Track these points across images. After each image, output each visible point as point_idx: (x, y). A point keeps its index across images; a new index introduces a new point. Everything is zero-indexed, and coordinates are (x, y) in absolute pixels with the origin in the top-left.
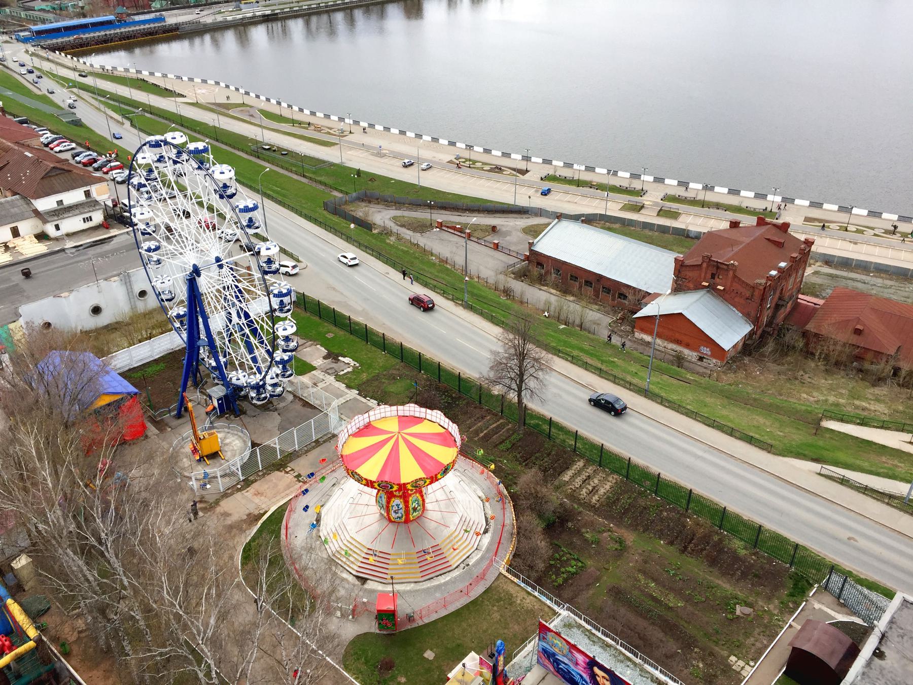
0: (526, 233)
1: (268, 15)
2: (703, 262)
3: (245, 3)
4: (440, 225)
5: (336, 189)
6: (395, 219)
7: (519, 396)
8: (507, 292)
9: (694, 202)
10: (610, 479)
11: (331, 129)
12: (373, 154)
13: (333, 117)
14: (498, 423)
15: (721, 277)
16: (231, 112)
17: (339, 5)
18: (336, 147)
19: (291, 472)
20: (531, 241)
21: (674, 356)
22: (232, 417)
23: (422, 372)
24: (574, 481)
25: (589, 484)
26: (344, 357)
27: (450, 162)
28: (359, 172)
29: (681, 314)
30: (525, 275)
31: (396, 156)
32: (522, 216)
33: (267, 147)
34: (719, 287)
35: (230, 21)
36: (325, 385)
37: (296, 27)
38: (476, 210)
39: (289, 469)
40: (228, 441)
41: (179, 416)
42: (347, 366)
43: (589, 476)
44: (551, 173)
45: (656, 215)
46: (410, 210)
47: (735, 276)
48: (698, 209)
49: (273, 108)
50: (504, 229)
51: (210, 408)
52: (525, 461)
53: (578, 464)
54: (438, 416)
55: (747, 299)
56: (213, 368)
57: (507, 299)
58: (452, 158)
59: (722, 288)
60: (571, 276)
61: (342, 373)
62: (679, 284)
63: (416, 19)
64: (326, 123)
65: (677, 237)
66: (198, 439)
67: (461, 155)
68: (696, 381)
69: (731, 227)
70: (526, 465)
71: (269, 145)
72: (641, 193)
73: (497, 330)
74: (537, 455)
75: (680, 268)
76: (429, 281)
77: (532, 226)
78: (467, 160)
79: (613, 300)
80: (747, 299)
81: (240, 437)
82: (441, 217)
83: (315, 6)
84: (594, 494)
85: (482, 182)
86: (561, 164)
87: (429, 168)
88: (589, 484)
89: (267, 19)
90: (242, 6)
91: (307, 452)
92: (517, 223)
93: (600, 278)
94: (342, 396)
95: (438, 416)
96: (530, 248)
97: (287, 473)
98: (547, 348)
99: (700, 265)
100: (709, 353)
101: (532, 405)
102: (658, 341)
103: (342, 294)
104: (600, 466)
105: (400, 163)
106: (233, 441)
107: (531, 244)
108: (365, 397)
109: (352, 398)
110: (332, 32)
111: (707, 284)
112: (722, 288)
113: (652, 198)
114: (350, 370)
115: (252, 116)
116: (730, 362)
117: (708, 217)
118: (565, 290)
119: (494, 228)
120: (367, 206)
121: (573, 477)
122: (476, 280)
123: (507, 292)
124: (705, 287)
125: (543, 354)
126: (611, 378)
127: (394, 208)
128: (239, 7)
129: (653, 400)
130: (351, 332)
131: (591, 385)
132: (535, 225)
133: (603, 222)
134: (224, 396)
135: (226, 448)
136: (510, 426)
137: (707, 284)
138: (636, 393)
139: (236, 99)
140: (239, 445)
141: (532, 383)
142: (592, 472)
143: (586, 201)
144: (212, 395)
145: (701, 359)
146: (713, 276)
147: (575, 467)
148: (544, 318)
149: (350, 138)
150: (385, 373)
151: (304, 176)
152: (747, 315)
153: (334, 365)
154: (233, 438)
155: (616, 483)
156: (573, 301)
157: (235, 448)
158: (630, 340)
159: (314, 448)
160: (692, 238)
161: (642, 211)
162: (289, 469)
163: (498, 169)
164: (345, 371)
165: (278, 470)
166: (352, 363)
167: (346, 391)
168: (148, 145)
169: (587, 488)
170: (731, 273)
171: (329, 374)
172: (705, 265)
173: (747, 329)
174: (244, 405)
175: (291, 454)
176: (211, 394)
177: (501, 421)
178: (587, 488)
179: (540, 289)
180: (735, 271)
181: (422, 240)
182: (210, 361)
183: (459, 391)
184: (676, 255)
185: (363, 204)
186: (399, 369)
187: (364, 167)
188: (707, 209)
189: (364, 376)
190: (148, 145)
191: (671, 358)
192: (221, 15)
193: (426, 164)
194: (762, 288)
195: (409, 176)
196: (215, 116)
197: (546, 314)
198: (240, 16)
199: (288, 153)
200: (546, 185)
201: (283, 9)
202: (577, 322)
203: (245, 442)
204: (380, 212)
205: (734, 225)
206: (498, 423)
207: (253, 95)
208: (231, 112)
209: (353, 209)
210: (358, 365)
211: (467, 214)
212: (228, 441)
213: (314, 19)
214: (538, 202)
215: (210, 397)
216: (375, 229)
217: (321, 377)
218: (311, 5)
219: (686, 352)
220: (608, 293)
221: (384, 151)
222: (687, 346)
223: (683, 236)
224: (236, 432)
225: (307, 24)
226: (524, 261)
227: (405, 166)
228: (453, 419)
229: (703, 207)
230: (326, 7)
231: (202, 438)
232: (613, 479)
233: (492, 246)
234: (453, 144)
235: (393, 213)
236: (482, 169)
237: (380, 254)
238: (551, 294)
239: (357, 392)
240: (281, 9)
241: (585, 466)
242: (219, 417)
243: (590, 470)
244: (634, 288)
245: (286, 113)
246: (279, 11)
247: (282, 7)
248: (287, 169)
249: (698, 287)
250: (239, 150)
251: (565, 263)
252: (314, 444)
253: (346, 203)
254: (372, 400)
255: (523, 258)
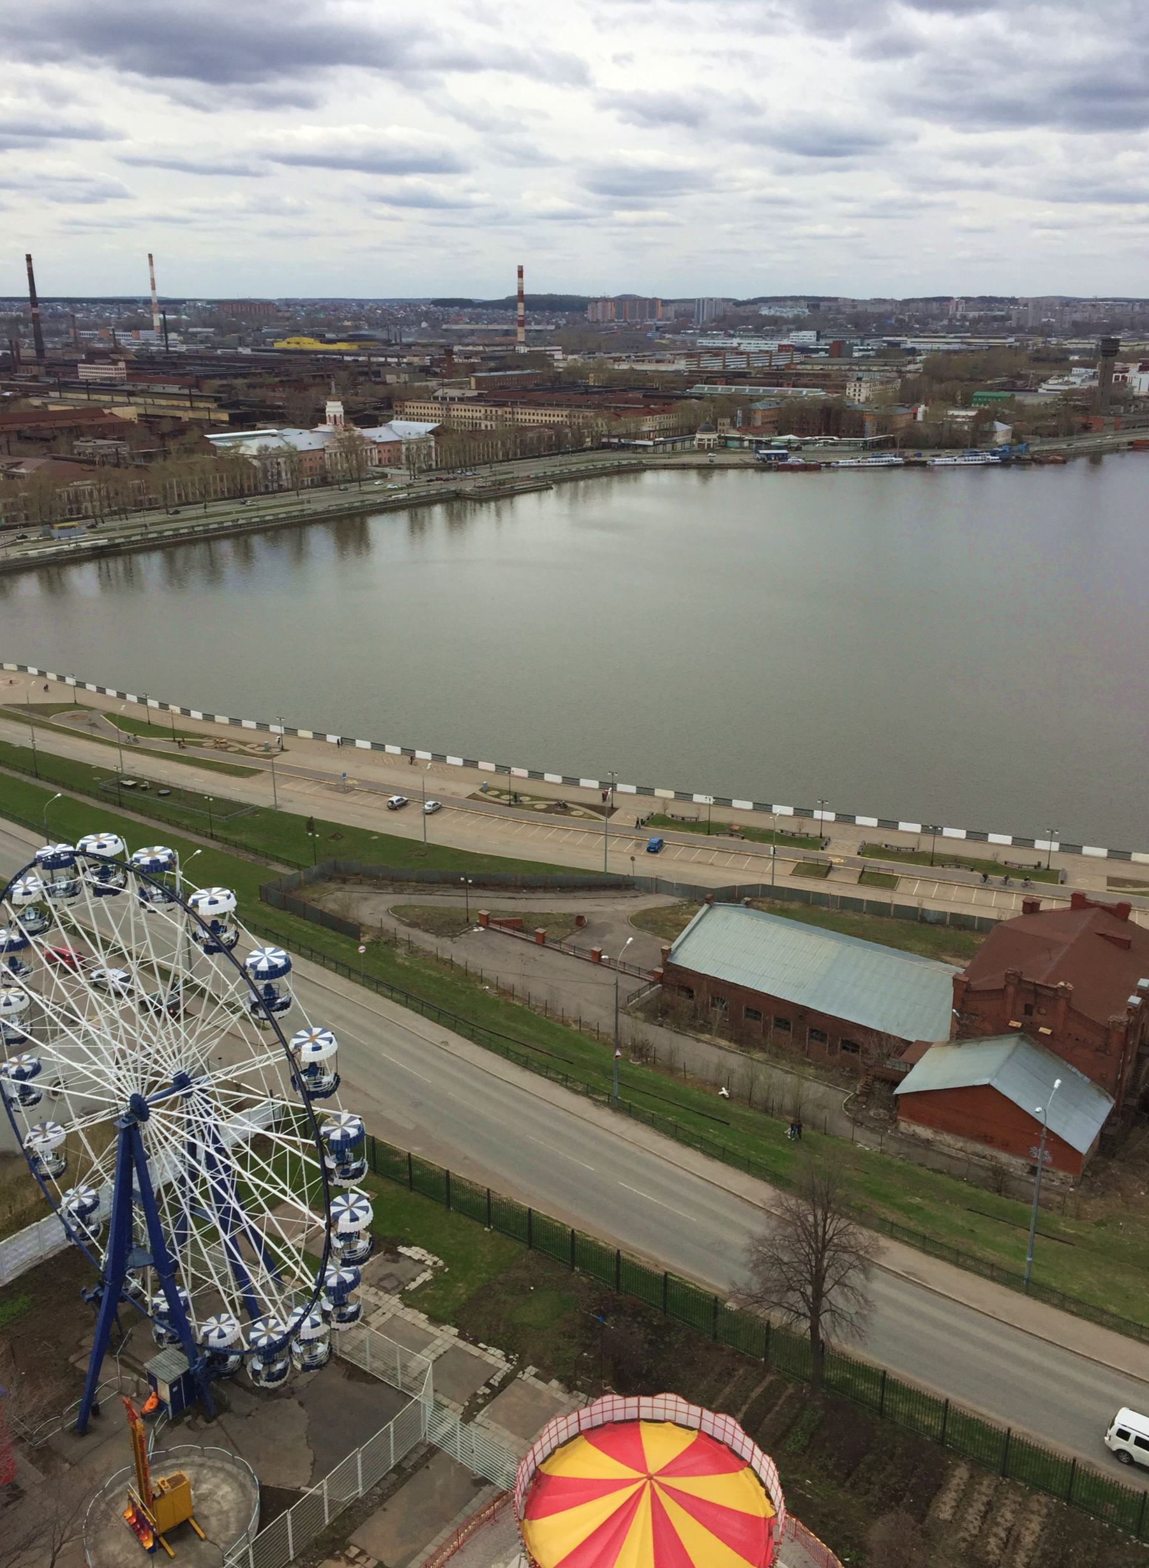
0: (639, 926)
1: (103, 547)
2: (1008, 984)
3: (60, 528)
4: (486, 921)
5: (278, 860)
6: (396, 910)
7: (814, 1329)
8: (641, 1050)
9: (914, 856)
10: (1035, 1506)
11: (245, 744)
12: (330, 788)
13: (246, 723)
14: (765, 1383)
15: (1043, 1011)
16: (53, 720)
17: (227, 528)
18: (258, 777)
19: (362, 1559)
20: (666, 947)
21: (988, 1169)
22: (201, 1422)
23: (577, 1269)
24: (963, 1519)
25: (998, 1524)
26: (409, 1245)
27: (474, 797)
28: (311, 823)
29: (988, 1087)
30: (665, 1014)
31: (375, 789)
32: (624, 893)
33: (130, 783)
34: (1042, 1030)
35: (33, 558)
36: (383, 1320)
37: (151, 565)
38: (540, 887)
39: (354, 1551)
40: (205, 1488)
41: (82, 1430)
42: (420, 1267)
43: (989, 1503)
44: (657, 810)
45: (856, 882)
46: (420, 891)
47: (1070, 1009)
48: (923, 869)
49: (129, 706)
50: (597, 921)
51: (150, 1405)
52: (848, 1475)
53: (957, 1473)
54: (729, 1429)
55: (1097, 1050)
56: (162, 1315)
57: (643, 1065)
58: (475, 789)
59: (1048, 1032)
60: (748, 1010)
61: (413, 1286)
62: (966, 1026)
63: (359, 553)
64: (233, 733)
65: (905, 921)
66: (150, 1499)
67: (492, 784)
68: (1081, 1237)
69: (1024, 911)
70: (853, 1486)
71: (133, 778)
72: (820, 842)
73: (761, 1191)
74: (869, 1458)
75: (964, 994)
76: (513, 1047)
77: (646, 912)
78: (502, 792)
79: (832, 1053)
80: (1097, 1050)
81: (230, 1474)
82: (486, 903)
83: (186, 531)
84: (1015, 1550)
85: (536, 832)
86: (671, 794)
87: (437, 809)
88: (998, 1524)
89: (98, 554)
90: (55, 532)
91: (384, 1498)
92: (620, 908)
93: (804, 1012)
94: (425, 1345)
95: (729, 1429)
96: (665, 960)
97: (352, 1561)
98: (864, 1218)
99: (1002, 991)
100: (1049, 1159)
101: (839, 1341)
102: (948, 1138)
103: (367, 1094)
104: (1004, 1476)
105: (382, 803)
106: (217, 1486)
107: (667, 953)
108: (475, 1343)
109: (447, 1347)
110: (213, 571)
111: (1019, 1024)
112: (1048, 1032)
113: (841, 850)
114: (427, 1276)
115: (93, 725)
116: (1089, 1174)
117: (945, 882)
118: (743, 1040)
119: (580, 920)
120: (340, 890)
121: (961, 1506)
122: (575, 1027)
123: (641, 1050)
124: (1016, 1029)
125: (864, 1236)
126: (946, 1253)
127: (390, 890)
128: (49, 534)
129: (1044, 1301)
130: (412, 1184)
131: (914, 1274)
132: (650, 910)
133: (768, 900)
134: (183, 1375)
135: (204, 1509)
136: (791, 1390)
137: (1019, 1024)
138: (1004, 1284)
139: (61, 696)
140: (231, 1497)
141: (835, 1297)
142: (990, 1491)
143: (730, 861)
144: (159, 1374)
145: (1033, 1171)
146: (1028, 1010)
147: (955, 1481)
148: (724, 1102)
149: (282, 759)
150: (501, 1277)
151: (212, 837)
152: (1103, 1083)
153: (391, 1268)
154: (214, 1480)
155: (1049, 1515)
156: (766, 1062)
157: (226, 1507)
158: (891, 1138)
159: (395, 1487)
160: (931, 923)
161: (831, 876)
162: (354, 1551)
163: (562, 807)
164: (419, 1280)
165: (330, 1555)
166: (430, 1260)
167: (432, 1329)
168: (40, 866)
169: (996, 1535)
170: (1062, 1005)
171: (387, 1291)
172: (1011, 989)
173: (1105, 1107)
174: (233, 1396)
175: (350, 1509)
176: (154, 1371)
177: (770, 1378)
178: (996, 1535)
179: (698, 1040)
180: (1068, 1000)
181: (459, 951)
182: (156, 1300)
183: (665, 1311)
184: (953, 969)
185: (332, 886)
186: (527, 1267)
187: (319, 814)
188: (940, 868)
189: (462, 1290)
190: (40, 866)
191: (983, 1174)
192: (18, 548)
193: (431, 803)
194: (1122, 1030)
195: (405, 826)
196: (25, 729)
197: (724, 1092)
198: (53, 549)
199: (174, 793)
200: (654, 834)
201: (130, 536)
202: (788, 1102)
203: (242, 1487)
204: (366, 899)
205: (1031, 908)
206: (765, 1383)
207: (91, 687)
208: (53, 720)
209: (316, 896)
210: (441, 1263)
211: (524, 894)
212: (205, 1488)
213: (180, 553)
214: (647, 866)
215: (152, 1380)
216: (365, 934)
217: (372, 1299)
218: (178, 529)
219: (1004, 1157)
220: (822, 1041)
221: (350, 782)
222: (1005, 1146)
223: (916, 919)
224: (219, 1464)
225: (170, 559)
226: (652, 984)
227: (394, 808)
228: (707, 1402)
229: (932, 865)
230: (206, 531)
231: (158, 1494)
232: (1040, 1503)
233: (588, 956)
234: (471, 764)
235: (391, 899)
236: (532, 808)
237: (407, 996)
238: (721, 1048)
239: (455, 1331)
240: (125, 537)
241: (972, 1477)
242: (173, 1423)
243: (986, 1486)
244: (878, 1033)
245: (159, 719)
246: (122, 540)
247: (127, 533)
248: (178, 825)
249: (1000, 1030)
250: (81, 792)
251: (735, 986)
252: (394, 1477)
253: (300, 885)
254: (492, 1350)
255: (651, 978)
